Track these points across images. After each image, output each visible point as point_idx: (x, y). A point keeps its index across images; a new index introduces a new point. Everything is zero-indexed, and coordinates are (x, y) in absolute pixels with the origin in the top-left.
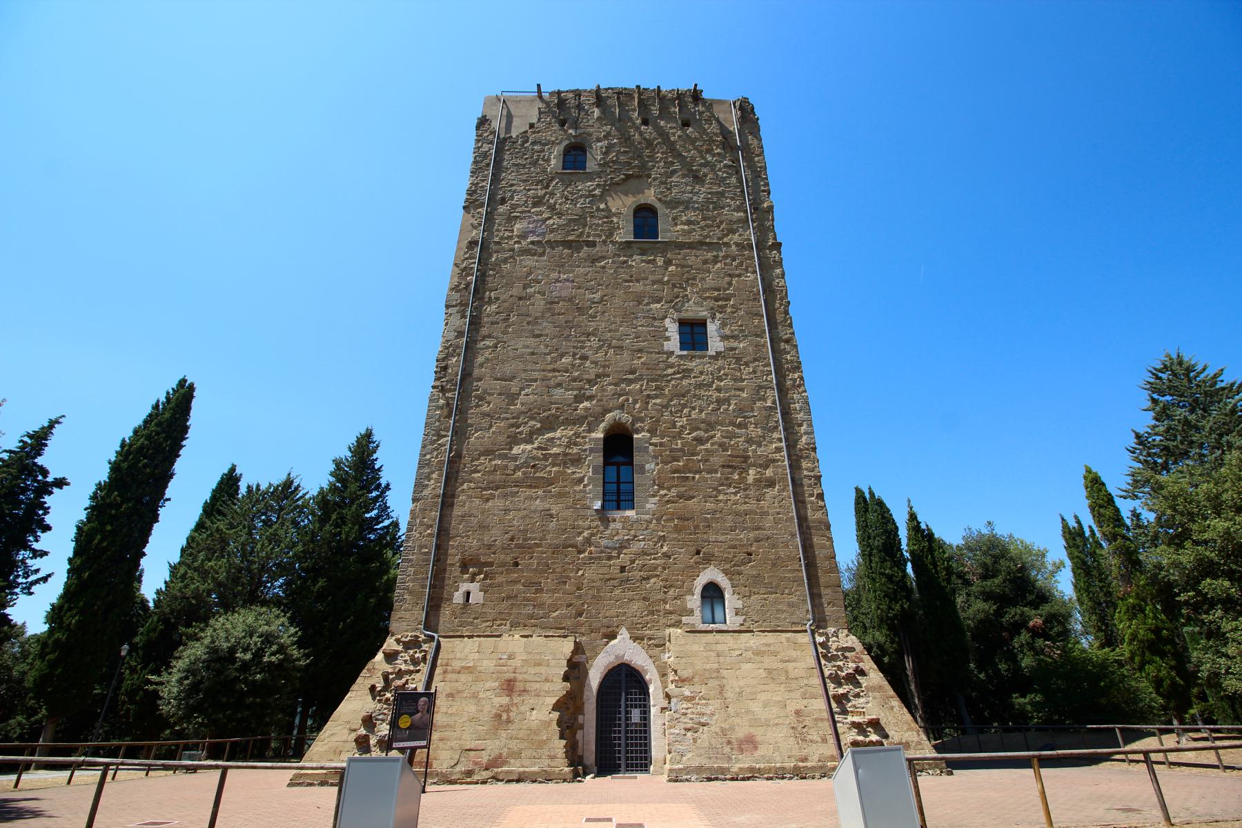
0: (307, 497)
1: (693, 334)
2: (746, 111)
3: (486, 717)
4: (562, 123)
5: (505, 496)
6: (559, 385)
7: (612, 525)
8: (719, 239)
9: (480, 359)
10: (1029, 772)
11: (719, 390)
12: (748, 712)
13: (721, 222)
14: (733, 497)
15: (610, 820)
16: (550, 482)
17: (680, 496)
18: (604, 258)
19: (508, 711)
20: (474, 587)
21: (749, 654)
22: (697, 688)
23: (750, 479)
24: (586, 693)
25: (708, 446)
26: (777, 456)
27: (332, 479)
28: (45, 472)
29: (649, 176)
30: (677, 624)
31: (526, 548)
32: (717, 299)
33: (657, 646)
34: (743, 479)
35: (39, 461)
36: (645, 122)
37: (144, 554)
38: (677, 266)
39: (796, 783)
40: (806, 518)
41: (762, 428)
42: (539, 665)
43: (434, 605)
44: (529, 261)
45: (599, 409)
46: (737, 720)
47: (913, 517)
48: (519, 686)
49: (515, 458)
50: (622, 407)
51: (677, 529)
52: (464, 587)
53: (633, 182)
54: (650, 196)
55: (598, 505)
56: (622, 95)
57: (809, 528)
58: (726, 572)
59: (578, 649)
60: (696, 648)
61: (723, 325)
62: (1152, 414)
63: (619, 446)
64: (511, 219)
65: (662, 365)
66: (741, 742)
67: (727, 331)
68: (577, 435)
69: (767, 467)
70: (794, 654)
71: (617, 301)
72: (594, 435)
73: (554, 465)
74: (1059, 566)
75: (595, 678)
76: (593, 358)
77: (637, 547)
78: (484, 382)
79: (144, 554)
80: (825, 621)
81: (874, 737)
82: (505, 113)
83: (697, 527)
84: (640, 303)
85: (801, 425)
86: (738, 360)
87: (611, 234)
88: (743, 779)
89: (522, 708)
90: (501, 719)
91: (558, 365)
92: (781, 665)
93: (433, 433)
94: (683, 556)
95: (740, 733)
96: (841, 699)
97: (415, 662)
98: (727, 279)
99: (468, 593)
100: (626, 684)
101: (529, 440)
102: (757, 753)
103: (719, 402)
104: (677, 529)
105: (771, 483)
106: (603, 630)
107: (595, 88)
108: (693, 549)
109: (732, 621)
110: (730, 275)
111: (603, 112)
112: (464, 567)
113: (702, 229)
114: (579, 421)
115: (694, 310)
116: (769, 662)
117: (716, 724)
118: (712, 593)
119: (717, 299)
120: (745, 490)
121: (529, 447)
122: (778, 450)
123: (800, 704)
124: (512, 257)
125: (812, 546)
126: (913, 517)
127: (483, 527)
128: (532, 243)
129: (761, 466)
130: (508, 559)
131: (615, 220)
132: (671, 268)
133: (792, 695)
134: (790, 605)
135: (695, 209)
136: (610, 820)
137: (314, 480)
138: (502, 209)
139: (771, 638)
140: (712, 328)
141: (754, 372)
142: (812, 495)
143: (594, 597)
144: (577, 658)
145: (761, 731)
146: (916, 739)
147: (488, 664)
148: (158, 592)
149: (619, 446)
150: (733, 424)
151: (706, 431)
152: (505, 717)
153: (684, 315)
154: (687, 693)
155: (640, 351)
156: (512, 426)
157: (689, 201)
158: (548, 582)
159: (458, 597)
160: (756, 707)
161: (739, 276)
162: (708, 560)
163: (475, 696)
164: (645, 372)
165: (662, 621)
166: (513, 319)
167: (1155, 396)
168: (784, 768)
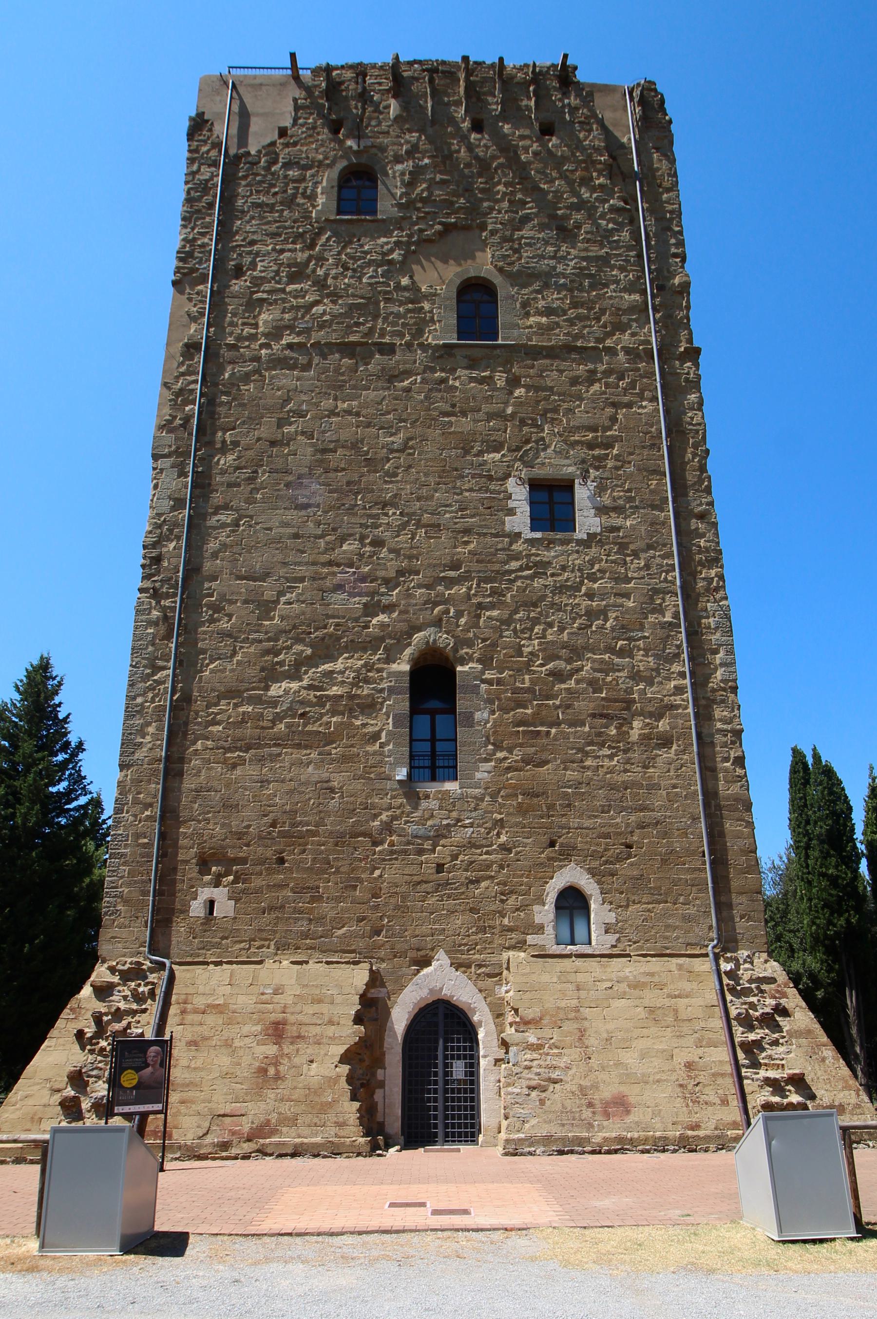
1: (552, 502)
3: (244, 1072)
4: (335, 128)
5: (261, 760)
6: (339, 587)
7: (424, 804)
8: (599, 340)
11: (590, 596)
12: (618, 1064)
13: (603, 311)
14: (607, 763)
15: (423, 1205)
16: (329, 739)
17: (527, 761)
18: (408, 373)
19: (276, 1064)
20: (220, 894)
21: (623, 987)
22: (547, 1033)
24: (388, 1040)
25: (572, 683)
26: (677, 700)
29: (483, 227)
30: (520, 945)
32: (591, 446)
33: (490, 976)
34: (623, 735)
36: (477, 126)
38: (528, 388)
39: (683, 1158)
40: (716, 794)
41: (656, 656)
42: (320, 1001)
43: (163, 918)
44: (286, 379)
45: (403, 626)
46: (603, 1076)
48: (292, 1030)
50: (438, 623)
51: (522, 810)
52: (205, 894)
54: (485, 263)
55: (402, 774)
57: (719, 808)
59: (375, 979)
60: (545, 978)
61: (601, 489)
63: (433, 684)
64: (253, 305)
65: (501, 556)
66: (607, 1104)
67: (606, 500)
68: (369, 667)
70: (687, 986)
72: (394, 667)
73: (334, 713)
75: (400, 1018)
76: (391, 543)
77: (459, 836)
80: (736, 941)
81: (795, 1098)
83: (551, 807)
84: (467, 452)
85: (716, 652)
86: (623, 547)
87: (420, 332)
88: (609, 1152)
89: (297, 1060)
90: (266, 1075)
91: (335, 555)
92: (667, 1002)
94: (530, 848)
95: (607, 1093)
96: (752, 1048)
98: (609, 411)
99: (212, 903)
100: (444, 1028)
101: (295, 676)
102: (629, 1119)
103: (591, 614)
105: (666, 742)
106: (411, 954)
107: (389, 60)
108: (545, 839)
109: (600, 941)
110: (614, 405)
111: (405, 107)
112: (204, 865)
113: (571, 322)
115: (554, 463)
116: (652, 998)
117: (573, 1080)
118: (572, 903)
119: (591, 446)
120: (625, 751)
121: (294, 685)
122: (680, 690)
123: (693, 1055)
124: (257, 371)
125: (722, 834)
127: (229, 806)
128: (290, 346)
129: (651, 715)
131: (426, 306)
132: (519, 392)
133: (683, 1042)
134: (687, 919)
135: (560, 288)
136: (423, 1205)
138: (237, 286)
139: (655, 965)
140: (582, 494)
141: (647, 567)
142: (727, 759)
143: (397, 907)
145: (636, 1089)
149: (433, 684)
150: (611, 650)
151: (569, 661)
152: (272, 1071)
153: (539, 472)
154: (532, 1039)
155: (467, 531)
157: (551, 273)
158: (329, 886)
159: (197, 908)
160: (629, 1058)
161: (629, 405)
163: (228, 1044)
164: (475, 566)
165: (498, 941)
166: (263, 478)
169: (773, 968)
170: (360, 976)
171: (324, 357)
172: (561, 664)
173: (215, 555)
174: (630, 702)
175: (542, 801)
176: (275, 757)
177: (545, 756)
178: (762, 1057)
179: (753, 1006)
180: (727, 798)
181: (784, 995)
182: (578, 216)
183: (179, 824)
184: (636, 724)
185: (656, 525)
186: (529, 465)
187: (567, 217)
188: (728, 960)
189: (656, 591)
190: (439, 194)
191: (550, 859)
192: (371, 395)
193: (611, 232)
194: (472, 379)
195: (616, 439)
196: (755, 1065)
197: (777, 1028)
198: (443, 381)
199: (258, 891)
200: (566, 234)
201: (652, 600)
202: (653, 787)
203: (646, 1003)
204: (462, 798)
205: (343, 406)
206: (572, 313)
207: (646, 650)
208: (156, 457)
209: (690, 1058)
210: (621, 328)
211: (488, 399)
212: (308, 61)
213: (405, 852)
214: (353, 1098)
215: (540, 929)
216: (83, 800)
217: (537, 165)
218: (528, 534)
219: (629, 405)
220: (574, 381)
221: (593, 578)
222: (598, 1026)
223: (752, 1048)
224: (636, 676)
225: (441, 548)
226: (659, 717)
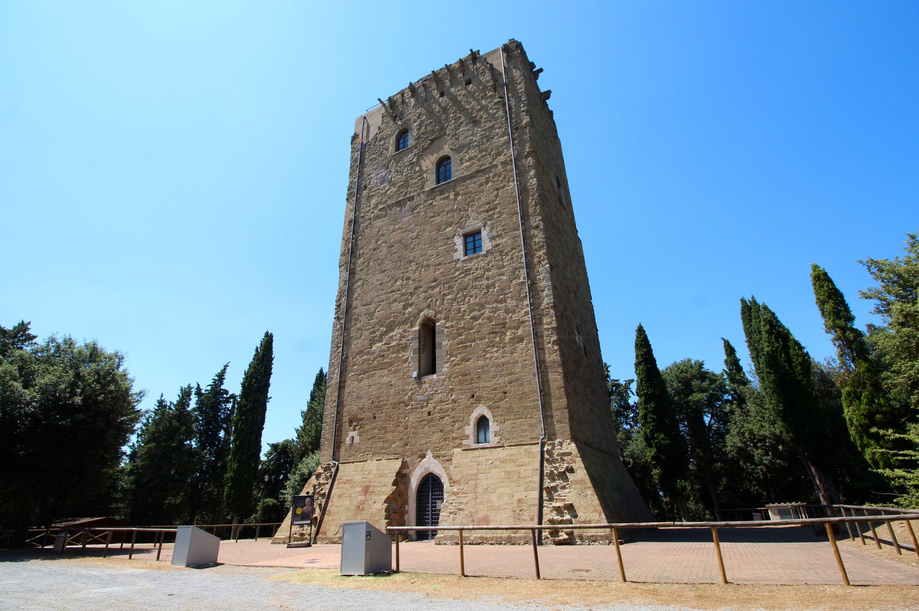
1: (472, 239)
2: (514, 50)
4: (394, 119)
5: (369, 377)
6: (395, 300)
7: (424, 386)
8: (490, 163)
9: (356, 295)
10: (711, 545)
11: (488, 279)
12: (489, 500)
13: (492, 150)
14: (496, 354)
16: (391, 364)
17: (462, 360)
18: (418, 205)
19: (363, 504)
20: (354, 434)
22: (461, 487)
23: (507, 339)
24: (410, 492)
25: (480, 321)
26: (526, 318)
28: (226, 392)
29: (445, 134)
30: (459, 446)
31: (379, 407)
32: (487, 211)
33: (448, 461)
34: (502, 340)
35: (223, 387)
36: (442, 95)
38: (462, 195)
39: (509, 548)
40: (544, 361)
41: (516, 300)
43: (337, 445)
44: (378, 223)
45: (416, 311)
46: (481, 507)
48: (371, 489)
49: (373, 353)
50: (429, 307)
51: (461, 383)
52: (351, 434)
53: (436, 143)
54: (446, 150)
55: (415, 374)
56: (425, 82)
57: (546, 367)
58: (489, 408)
59: (404, 465)
60: (466, 460)
61: (492, 229)
64: (369, 198)
65: (452, 271)
67: (494, 233)
68: (405, 331)
69: (519, 327)
70: (527, 460)
71: (427, 234)
72: (414, 329)
73: (393, 353)
75: (414, 482)
76: (412, 278)
77: (437, 398)
78: (359, 309)
80: (555, 435)
81: (567, 517)
82: (365, 126)
83: (472, 379)
84: (439, 231)
85: (543, 291)
86: (501, 252)
87: (423, 187)
88: (476, 544)
91: (394, 288)
92: (516, 469)
93: (335, 345)
94: (464, 400)
96: (550, 490)
97: (327, 479)
98: (495, 192)
100: (431, 486)
101: (380, 341)
103: (488, 287)
104: (461, 383)
105: (521, 340)
106: (419, 453)
107: (408, 85)
108: (469, 395)
109: (493, 440)
110: (497, 189)
111: (416, 100)
112: (351, 422)
113: (479, 160)
114: (404, 323)
115: (472, 224)
116: (509, 467)
117: (468, 509)
118: (482, 423)
119: (487, 211)
120: (503, 348)
121: (380, 344)
122: (527, 313)
123: (522, 495)
124: (370, 223)
125: (548, 381)
127: (359, 398)
128: (380, 210)
129: (515, 328)
130: (371, 415)
131: (425, 175)
132: (459, 198)
133: (519, 489)
134: (531, 425)
135: (474, 147)
138: (365, 193)
139: (515, 450)
140: (484, 234)
141: (512, 258)
142: (549, 343)
143: (414, 433)
144: (405, 471)
145: (493, 513)
146: (597, 518)
147: (358, 478)
150: (496, 301)
151: (479, 310)
153: (467, 230)
154: (455, 490)
155: (440, 264)
156: (371, 333)
157: (471, 142)
158: (390, 427)
159: (348, 441)
160: (494, 497)
161: (503, 187)
162: (478, 401)
164: (442, 278)
165: (451, 444)
166: (371, 264)
168: (501, 538)
169: (572, 447)
170: (397, 464)
171: (391, 210)
172: (476, 313)
173: (356, 299)
174: (504, 324)
175: (468, 377)
176: (373, 375)
177: (469, 356)
178: (555, 496)
179: (556, 468)
180: (550, 362)
181: (574, 462)
182: (481, 113)
183: (344, 407)
184: (508, 333)
185: (515, 238)
186: (463, 228)
187: (476, 116)
188: (549, 445)
189: (516, 269)
190: (429, 128)
191: (472, 404)
192: (406, 219)
193: (494, 114)
194: (441, 199)
195: (498, 204)
196: (551, 499)
197: (566, 479)
198: (431, 204)
200: (476, 122)
201: (514, 274)
202: (517, 362)
203: (507, 470)
204: (438, 381)
205: (397, 227)
206: (479, 156)
207: (512, 298)
208: (340, 267)
210: (499, 154)
211: (447, 205)
212: (385, 99)
213: (417, 408)
214: (386, 518)
215: (467, 437)
217: (465, 99)
218: (463, 258)
219: (503, 187)
220: (481, 185)
221: (489, 270)
222: (484, 482)
223: (550, 490)
224: (507, 311)
225: (429, 274)
226: (517, 328)
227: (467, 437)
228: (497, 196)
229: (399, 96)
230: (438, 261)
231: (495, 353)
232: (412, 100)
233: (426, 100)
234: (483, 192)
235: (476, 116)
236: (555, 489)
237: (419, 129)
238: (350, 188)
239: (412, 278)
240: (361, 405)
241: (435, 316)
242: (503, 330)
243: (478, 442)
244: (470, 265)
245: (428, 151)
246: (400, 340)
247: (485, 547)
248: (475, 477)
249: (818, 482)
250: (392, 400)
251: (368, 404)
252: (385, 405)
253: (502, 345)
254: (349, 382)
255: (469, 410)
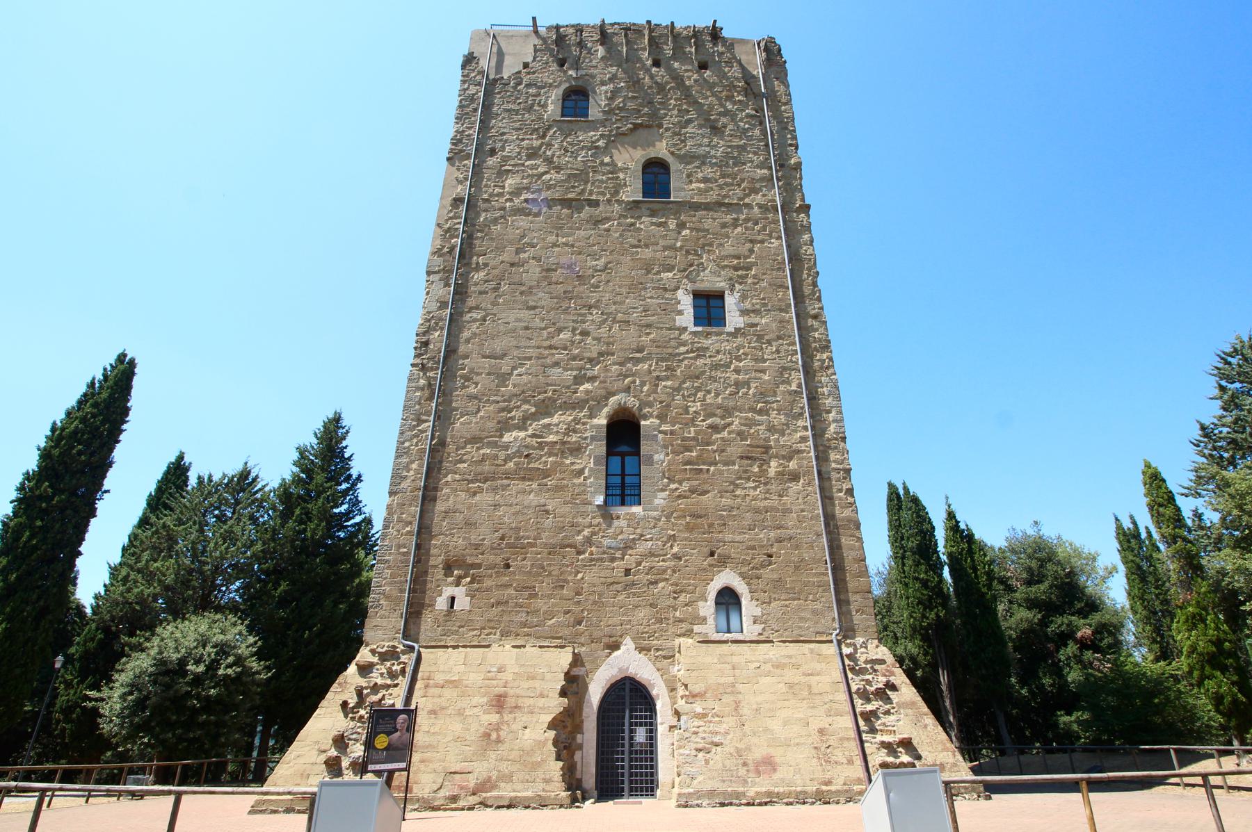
0: (267, 489)
1: (709, 307)
2: (772, 52)
4: (562, 63)
6: (557, 364)
7: (616, 523)
8: (740, 199)
11: (737, 371)
12: (766, 730)
14: (752, 492)
16: (546, 474)
17: (693, 491)
18: (608, 219)
19: (498, 729)
20: (460, 592)
21: (768, 667)
24: (586, 710)
25: (725, 434)
26: (802, 446)
27: (296, 469)
29: (660, 126)
30: (689, 633)
31: (519, 548)
32: (736, 269)
33: (665, 657)
34: (763, 472)
36: (657, 63)
37: (80, 554)
38: (691, 229)
39: (819, 808)
40: (833, 516)
41: (786, 415)
42: (533, 678)
43: (414, 611)
44: (523, 222)
45: (602, 392)
46: (754, 740)
47: (951, 516)
48: (510, 702)
49: (506, 447)
50: (627, 390)
51: (689, 528)
52: (448, 591)
53: (642, 133)
54: (661, 149)
55: (600, 500)
57: (837, 527)
58: (743, 576)
59: (577, 660)
60: (708, 660)
61: (744, 298)
62: (1219, 403)
63: (624, 434)
64: (501, 173)
66: (757, 764)
71: (623, 270)
72: (596, 421)
73: (550, 454)
74: (1111, 572)
75: (595, 692)
76: (595, 334)
77: (643, 547)
79: (80, 554)
80: (854, 630)
81: (905, 758)
82: (495, 49)
83: (711, 525)
84: (649, 272)
85: (829, 412)
86: (760, 337)
87: (617, 192)
88: (760, 804)
90: (490, 739)
91: (554, 342)
94: (696, 557)
95: (758, 754)
96: (869, 717)
97: (392, 675)
98: (748, 245)
99: (453, 599)
100: (630, 699)
102: (776, 776)
103: (738, 384)
105: (795, 477)
106: (605, 640)
108: (706, 550)
110: (751, 241)
111: (608, 51)
112: (448, 568)
115: (710, 280)
118: (728, 599)
119: (736, 269)
120: (766, 484)
121: (522, 434)
122: (804, 439)
123: (823, 722)
125: (839, 547)
126: (951, 516)
127: (470, 524)
129: (784, 457)
130: (498, 560)
131: (621, 176)
132: (685, 232)
137: (275, 470)
138: (491, 161)
139: (793, 649)
140: (730, 301)
141: (778, 351)
142: (840, 490)
143: (595, 603)
147: (475, 678)
148: (97, 597)
149: (624, 434)
150: (753, 410)
151: (723, 418)
152: (494, 736)
154: (699, 710)
155: (649, 326)
156: (503, 410)
158: (543, 587)
159: (441, 603)
162: (723, 562)
163: (460, 713)
164: (654, 350)
165: (672, 630)
166: (504, 288)
167: (1223, 383)
169: (883, 652)
170: (565, 657)
172: (716, 420)
173: (468, 341)
176: (505, 487)
177: (706, 487)
180: (842, 520)
181: (893, 674)
183: (432, 537)
184: (773, 464)
190: (630, 105)
191: (711, 565)
192: (582, 233)
197: (888, 700)
198: (632, 224)
199: (488, 590)
202: (789, 511)
203: (786, 679)
204: (644, 518)
205: (561, 240)
206: (721, 181)
207: (779, 410)
208: (429, 273)
209: (822, 726)
212: (543, 23)
213: (601, 560)
215: (704, 620)
216: (358, 519)
218: (692, 328)
219: (762, 242)
221: (739, 359)
225: (631, 337)
227: (704, 620)
228: (751, 251)
229: (572, 31)
230: (646, 320)
231: (751, 492)
232: (600, 48)
233: (627, 60)
234: (728, 237)
235: (716, 121)
236: (874, 713)
237: (612, 99)
238: (456, 142)
239: (595, 334)
240: (474, 538)
241: (640, 409)
242: (765, 457)
243: (729, 631)
244: (706, 342)
245: (627, 139)
246: (566, 434)
247: (779, 810)
248: (732, 689)
249: (951, 718)
250: (546, 538)
251: (490, 539)
252: (532, 545)
253: (762, 479)
254: (446, 491)
255: (705, 575)
